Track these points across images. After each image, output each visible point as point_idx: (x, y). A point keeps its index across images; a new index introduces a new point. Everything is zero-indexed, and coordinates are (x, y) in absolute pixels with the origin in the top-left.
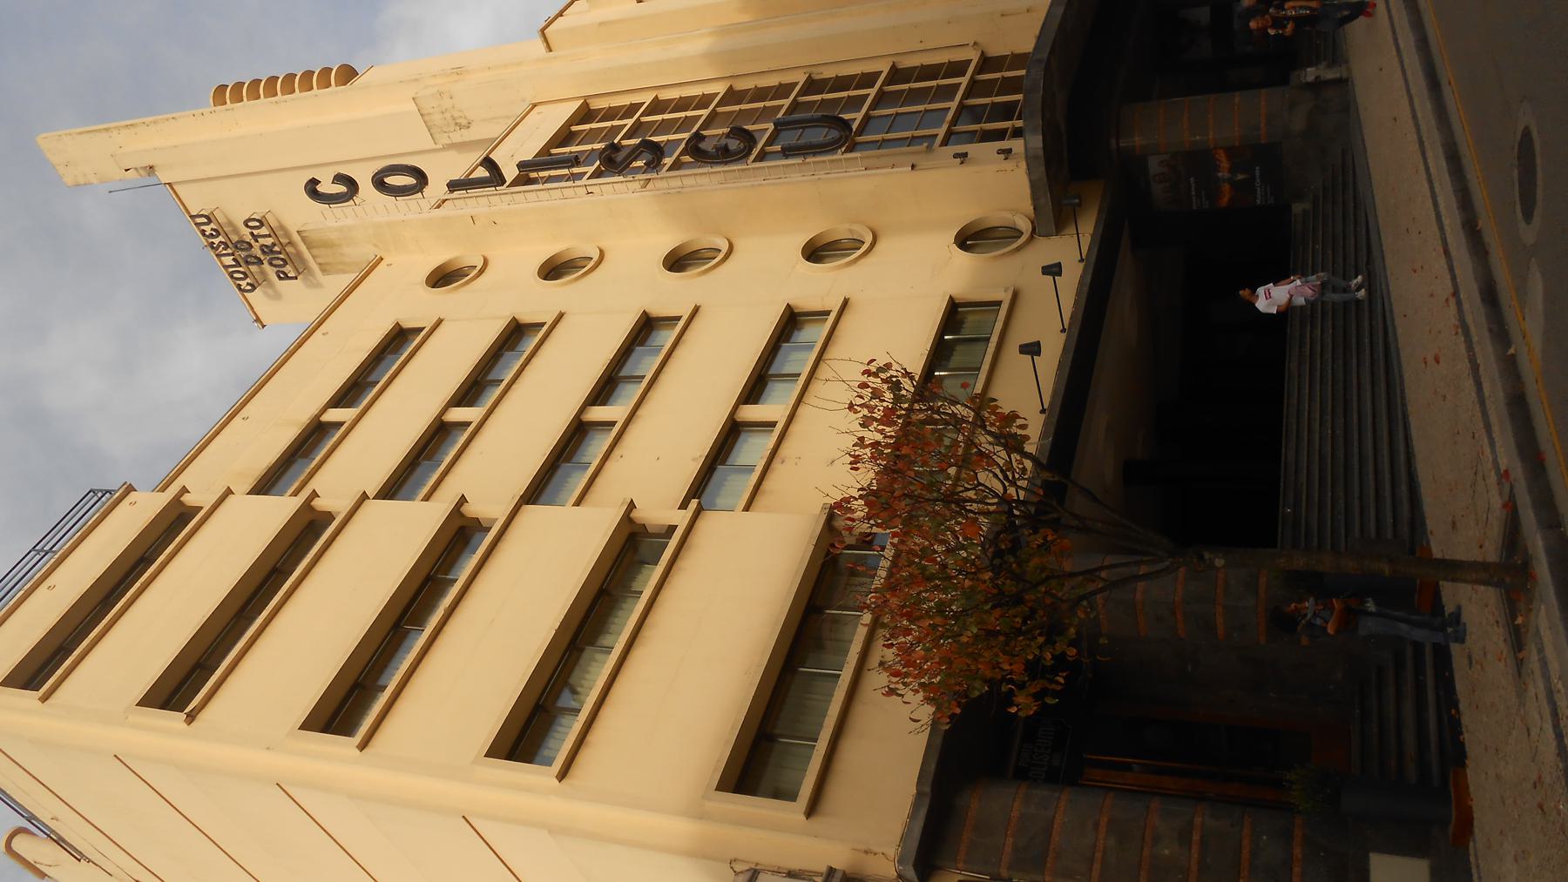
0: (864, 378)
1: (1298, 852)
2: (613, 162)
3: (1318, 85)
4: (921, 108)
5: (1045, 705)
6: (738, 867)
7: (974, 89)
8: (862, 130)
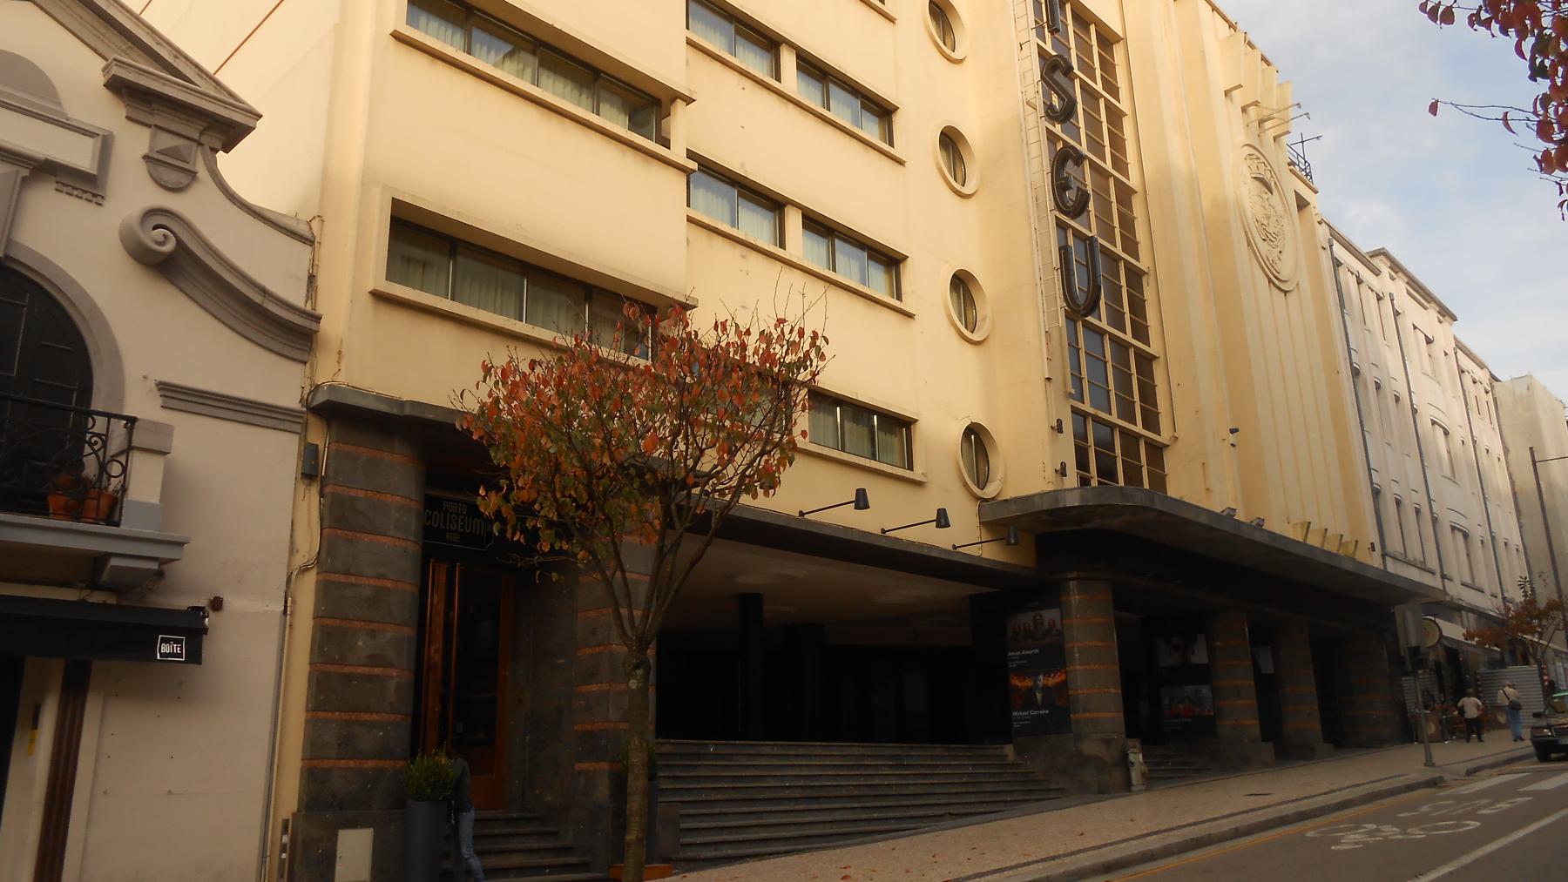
0: (808, 334)
1: (370, 764)
2: (1054, 69)
3: (1126, 764)
4: (1112, 386)
5: (489, 522)
6: (315, 224)
7: (1130, 438)
8: (1088, 327)
